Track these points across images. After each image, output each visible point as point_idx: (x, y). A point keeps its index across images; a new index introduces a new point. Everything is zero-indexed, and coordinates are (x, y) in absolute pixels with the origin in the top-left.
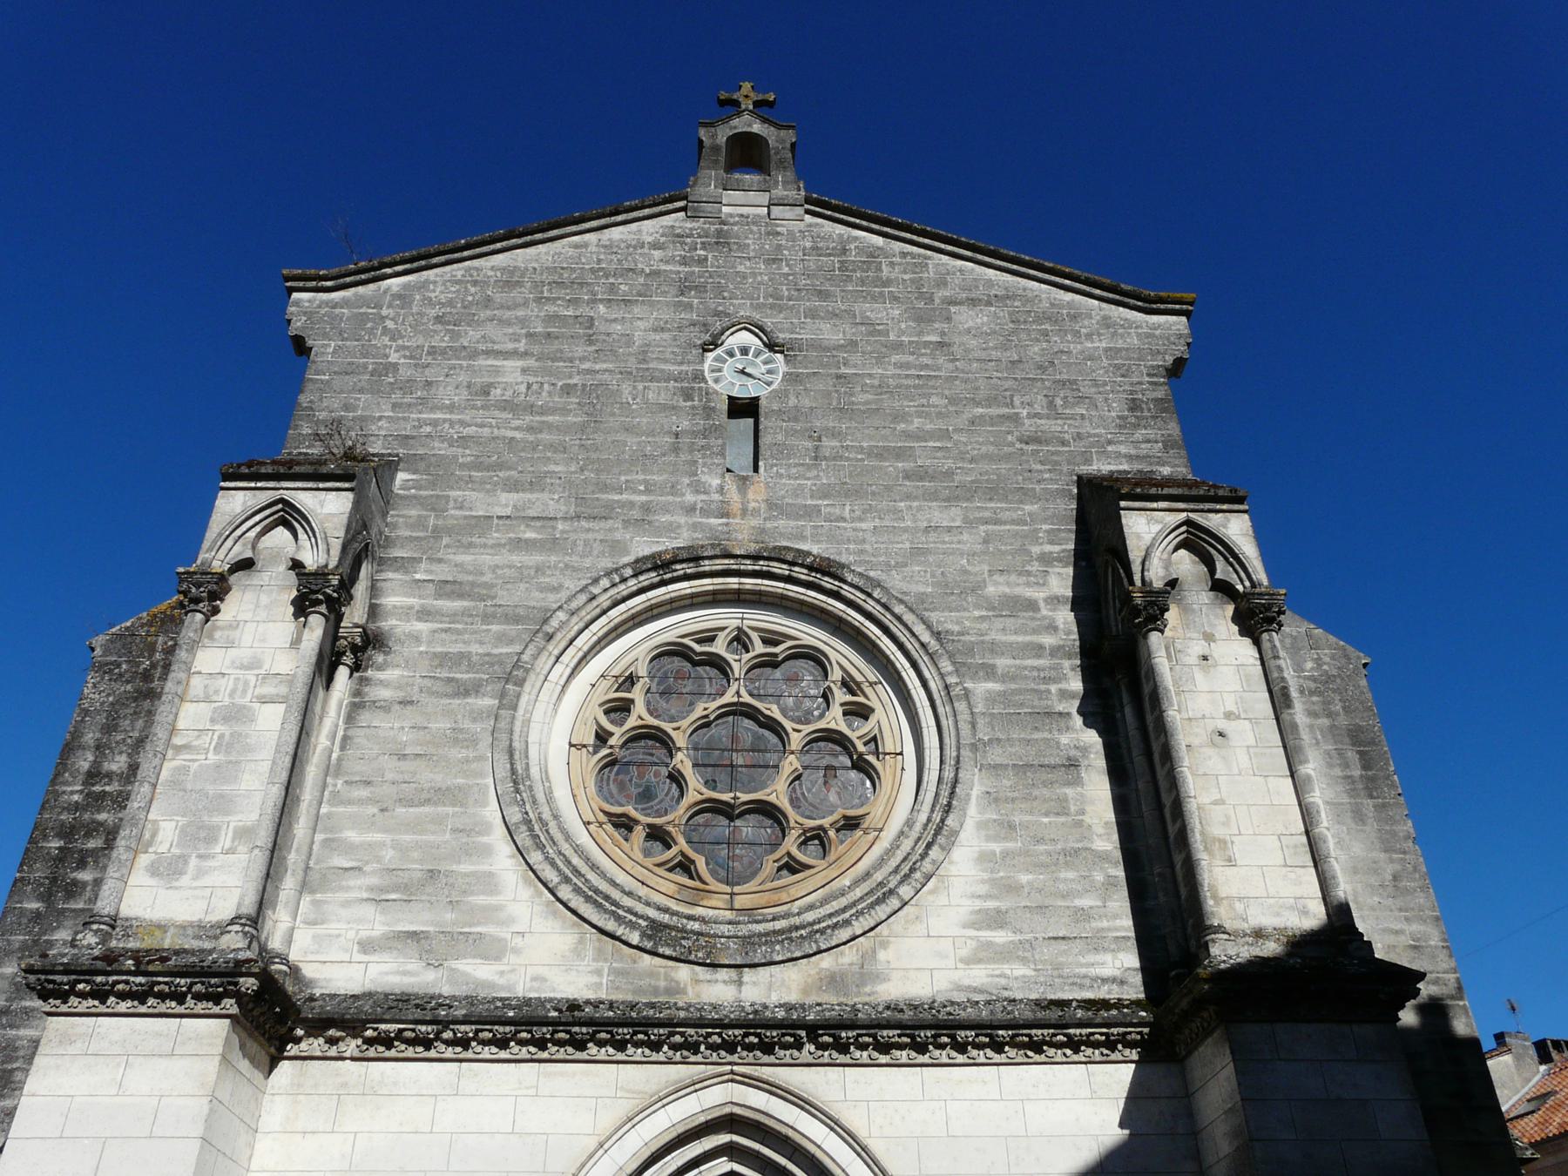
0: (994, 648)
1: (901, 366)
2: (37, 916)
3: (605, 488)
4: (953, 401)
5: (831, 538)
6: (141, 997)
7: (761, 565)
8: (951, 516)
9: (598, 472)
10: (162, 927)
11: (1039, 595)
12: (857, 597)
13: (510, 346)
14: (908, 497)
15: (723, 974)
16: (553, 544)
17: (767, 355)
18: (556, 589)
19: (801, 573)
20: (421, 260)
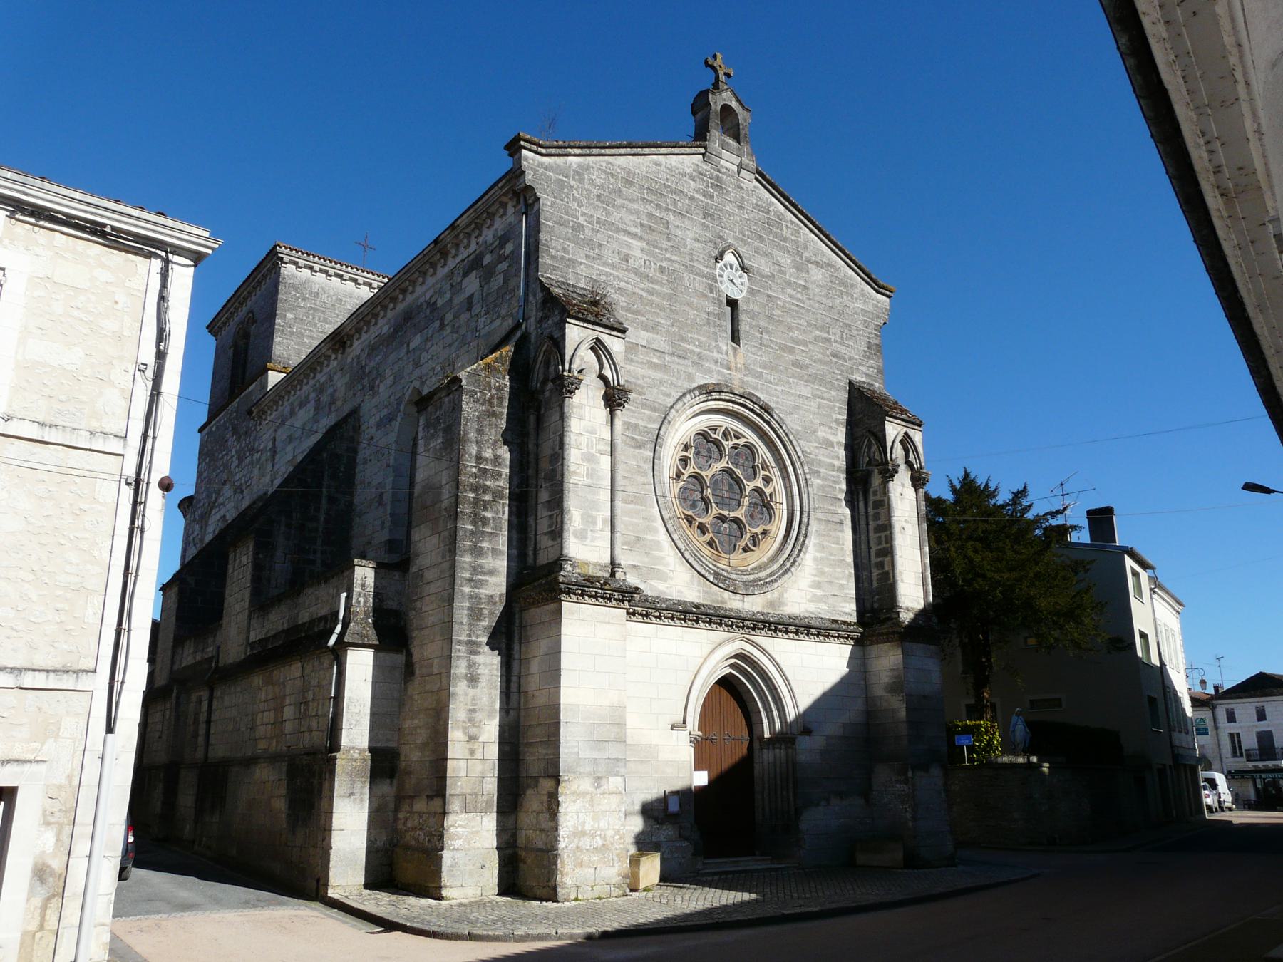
0: (820, 463)
1: (791, 297)
2: (472, 533)
3: (683, 339)
4: (809, 324)
5: (767, 393)
6: (596, 597)
7: (742, 401)
8: (806, 391)
9: (680, 328)
10: (587, 564)
11: (832, 438)
12: (776, 426)
13: (633, 230)
14: (793, 376)
15: (739, 597)
16: (664, 368)
17: (740, 272)
18: (669, 395)
19: (757, 408)
20: (588, 147)
